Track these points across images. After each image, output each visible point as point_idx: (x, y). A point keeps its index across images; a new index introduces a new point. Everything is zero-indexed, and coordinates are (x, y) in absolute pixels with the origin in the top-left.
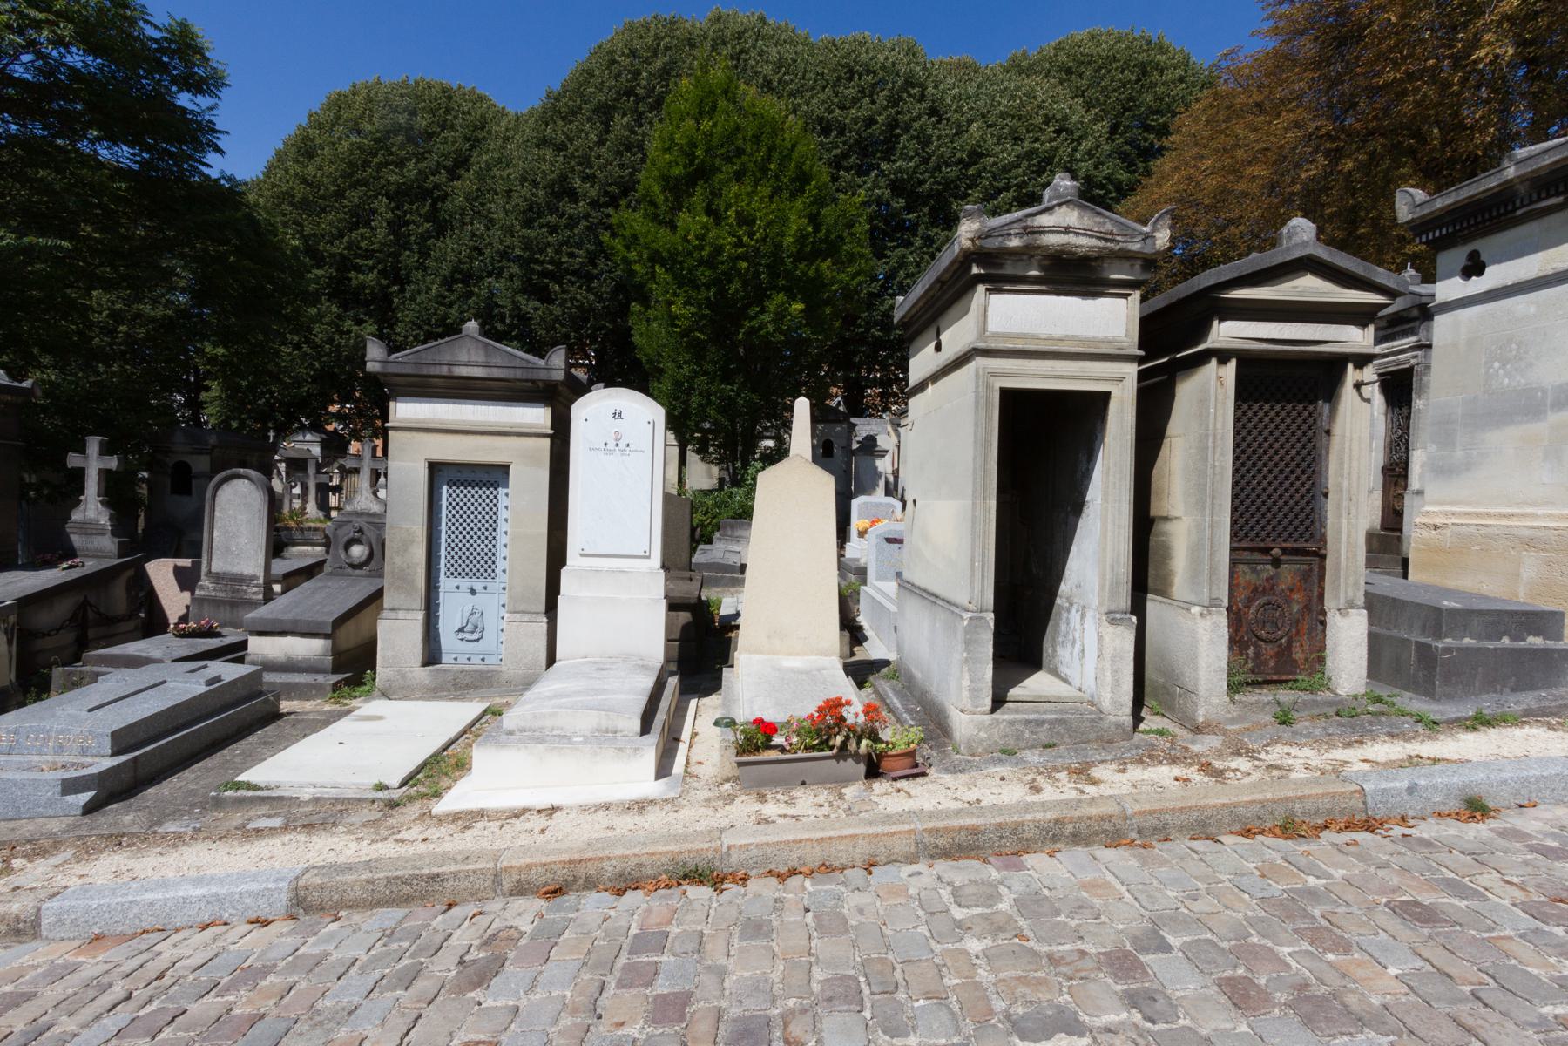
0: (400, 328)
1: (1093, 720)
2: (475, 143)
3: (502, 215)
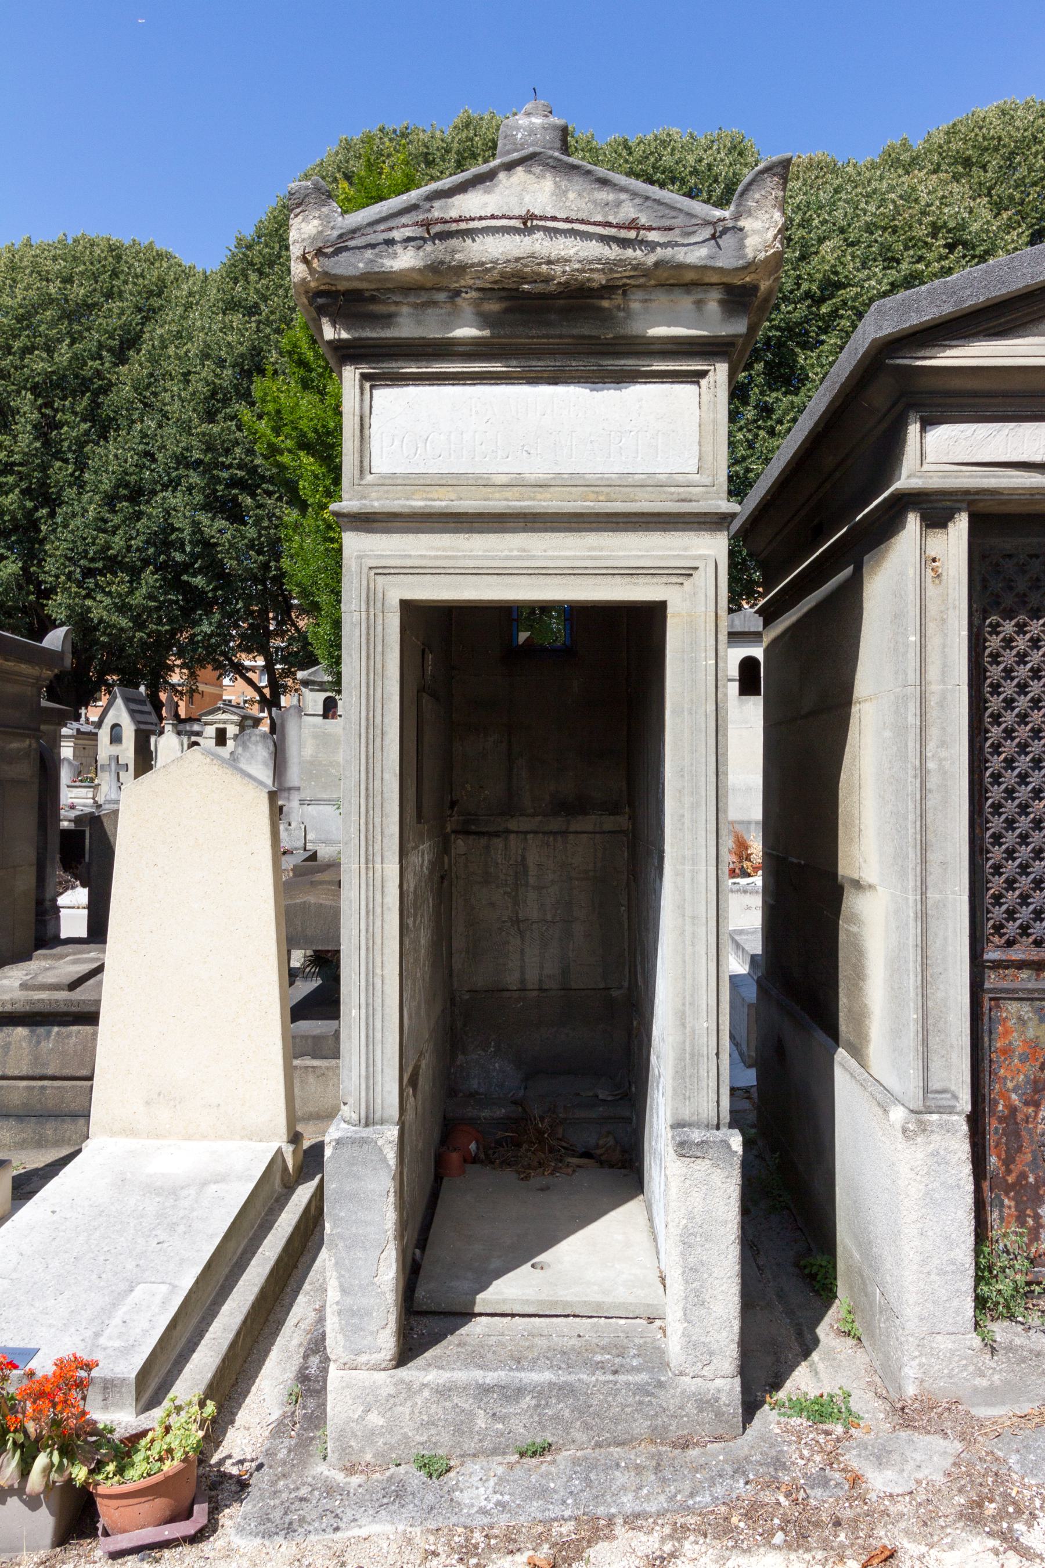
0: (50, 565)
1: (641, 1389)
2: (149, 314)
3: (177, 404)
